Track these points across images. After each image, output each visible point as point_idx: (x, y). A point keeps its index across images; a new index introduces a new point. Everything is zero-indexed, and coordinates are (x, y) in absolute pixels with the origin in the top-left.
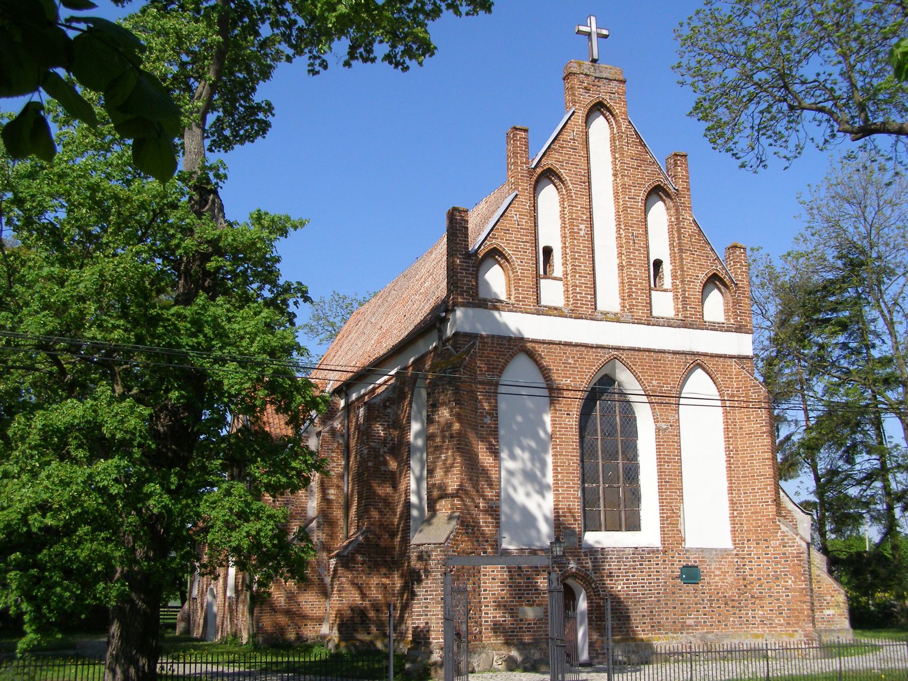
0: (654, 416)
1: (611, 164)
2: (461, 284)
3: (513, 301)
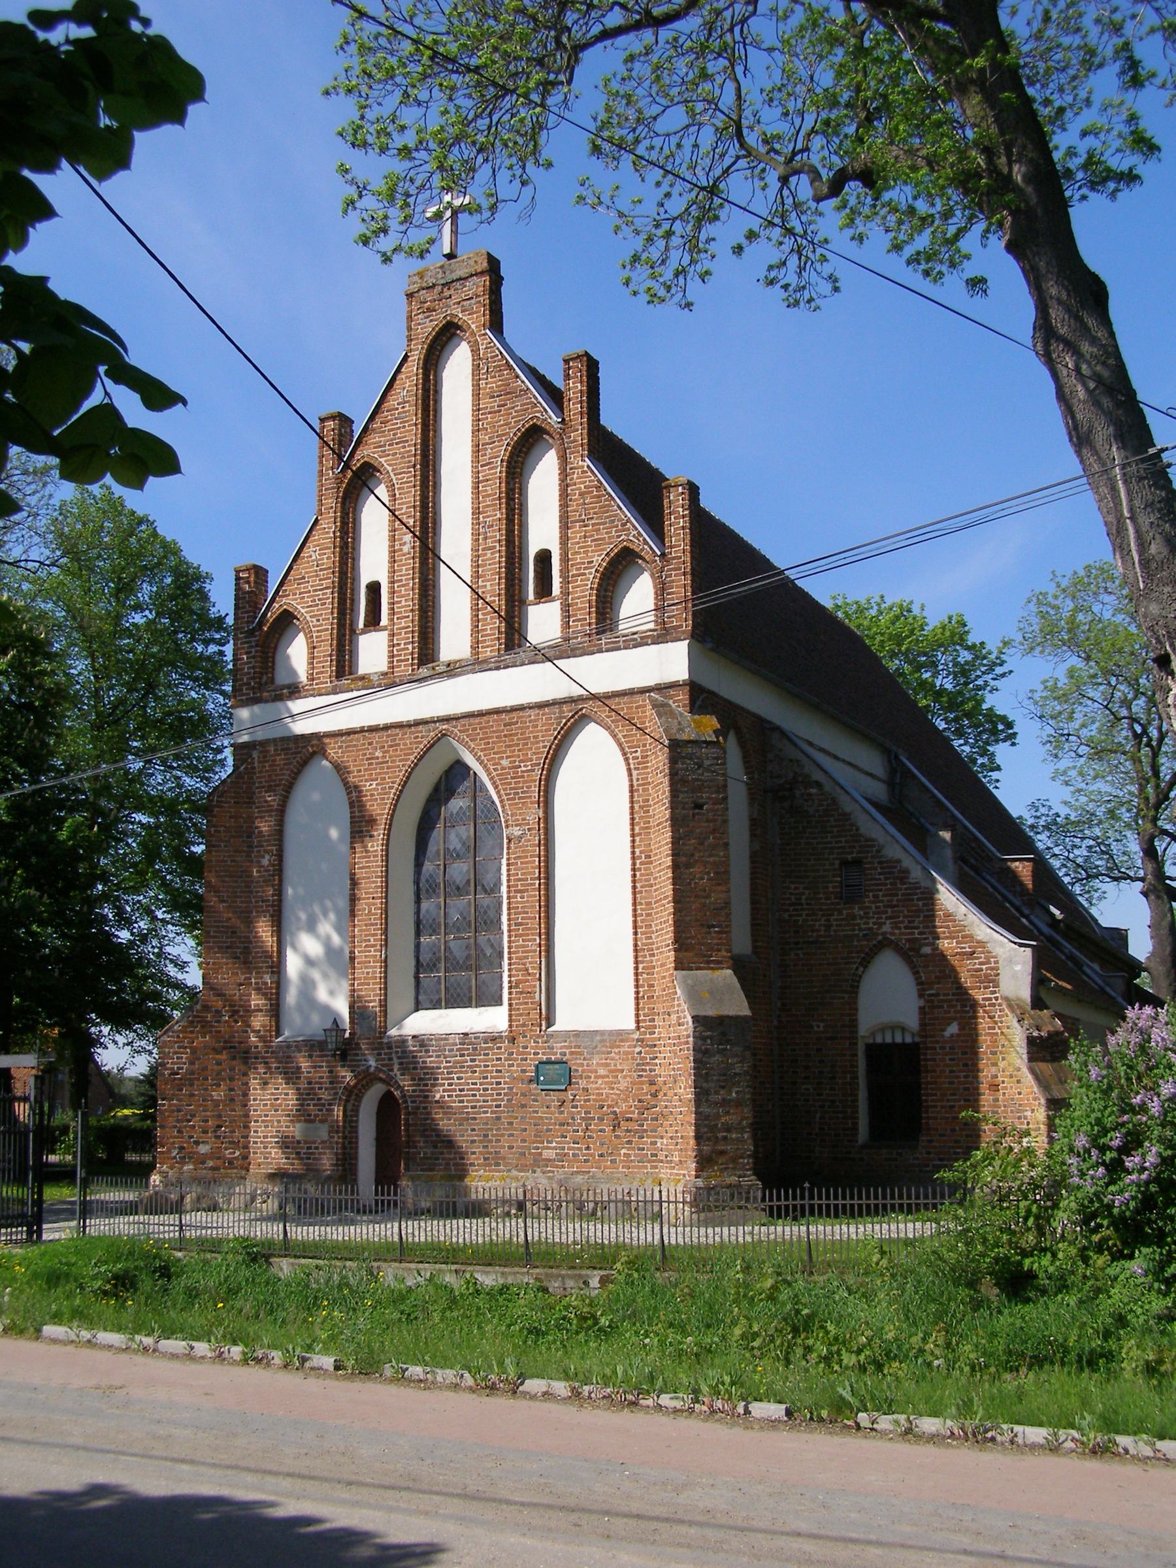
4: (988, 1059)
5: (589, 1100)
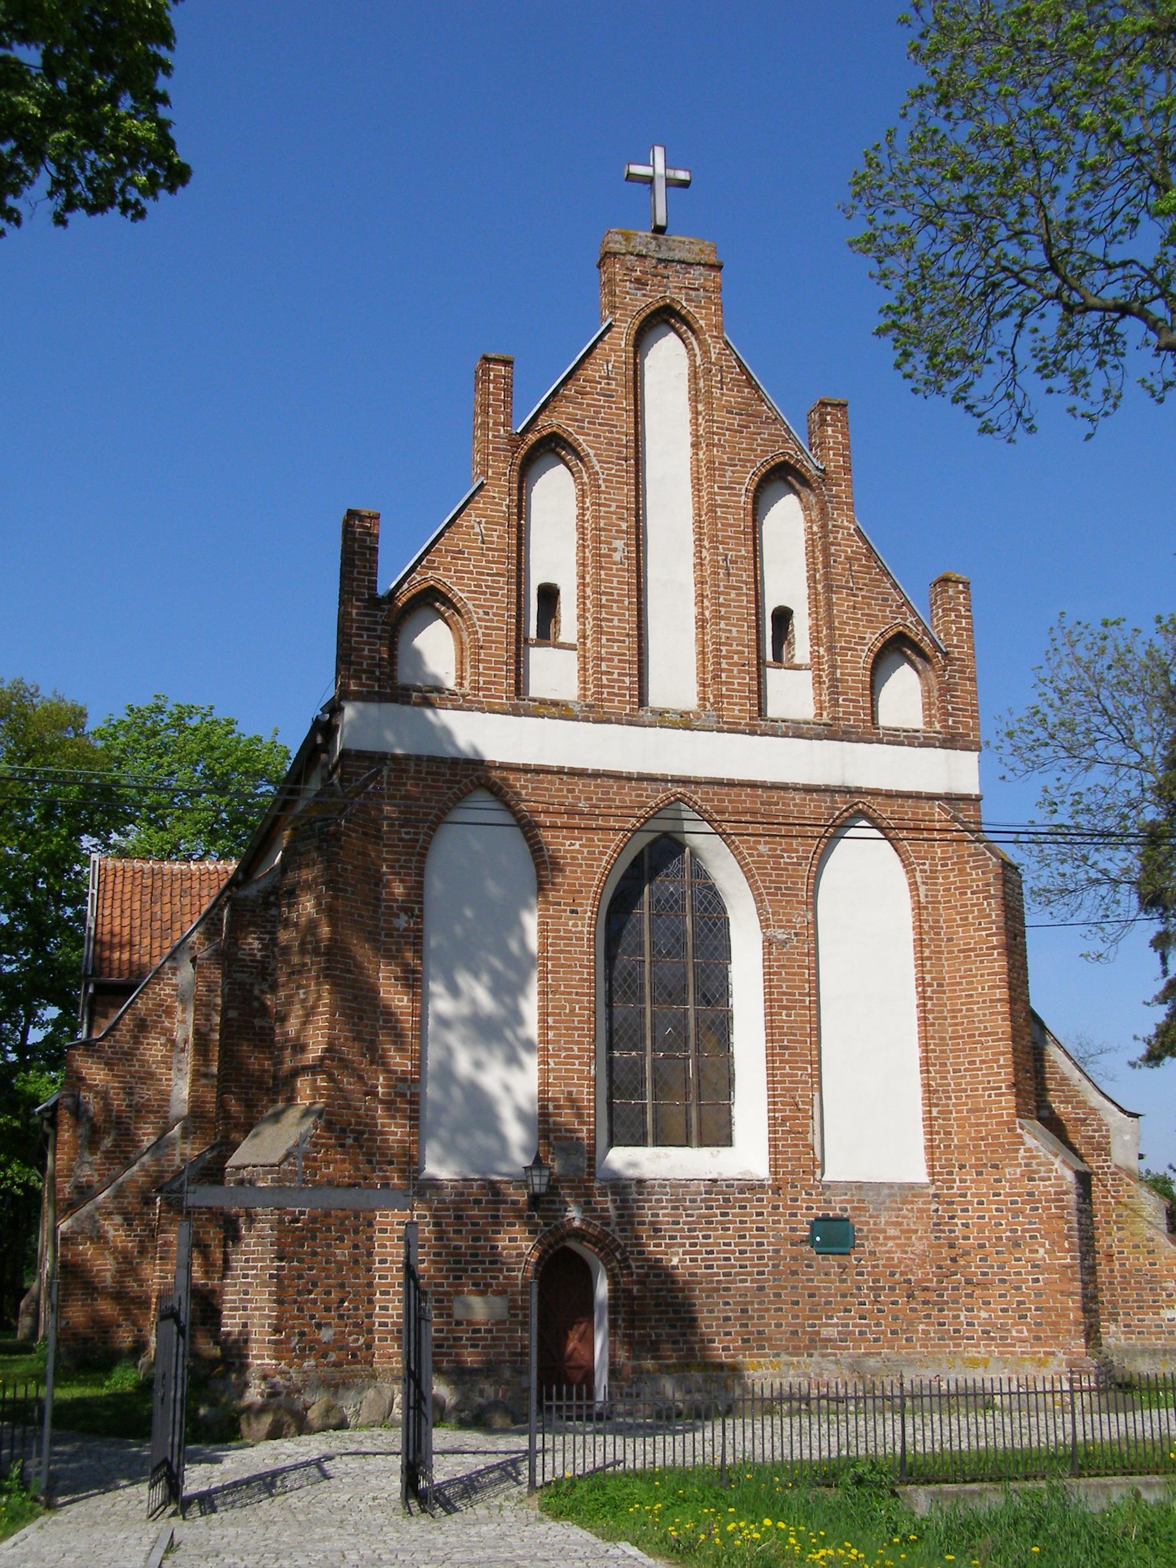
0: (760, 915)
1: (688, 424)
2: (358, 656)
3: (467, 688)
4: (1104, 1228)
5: (877, 1266)
